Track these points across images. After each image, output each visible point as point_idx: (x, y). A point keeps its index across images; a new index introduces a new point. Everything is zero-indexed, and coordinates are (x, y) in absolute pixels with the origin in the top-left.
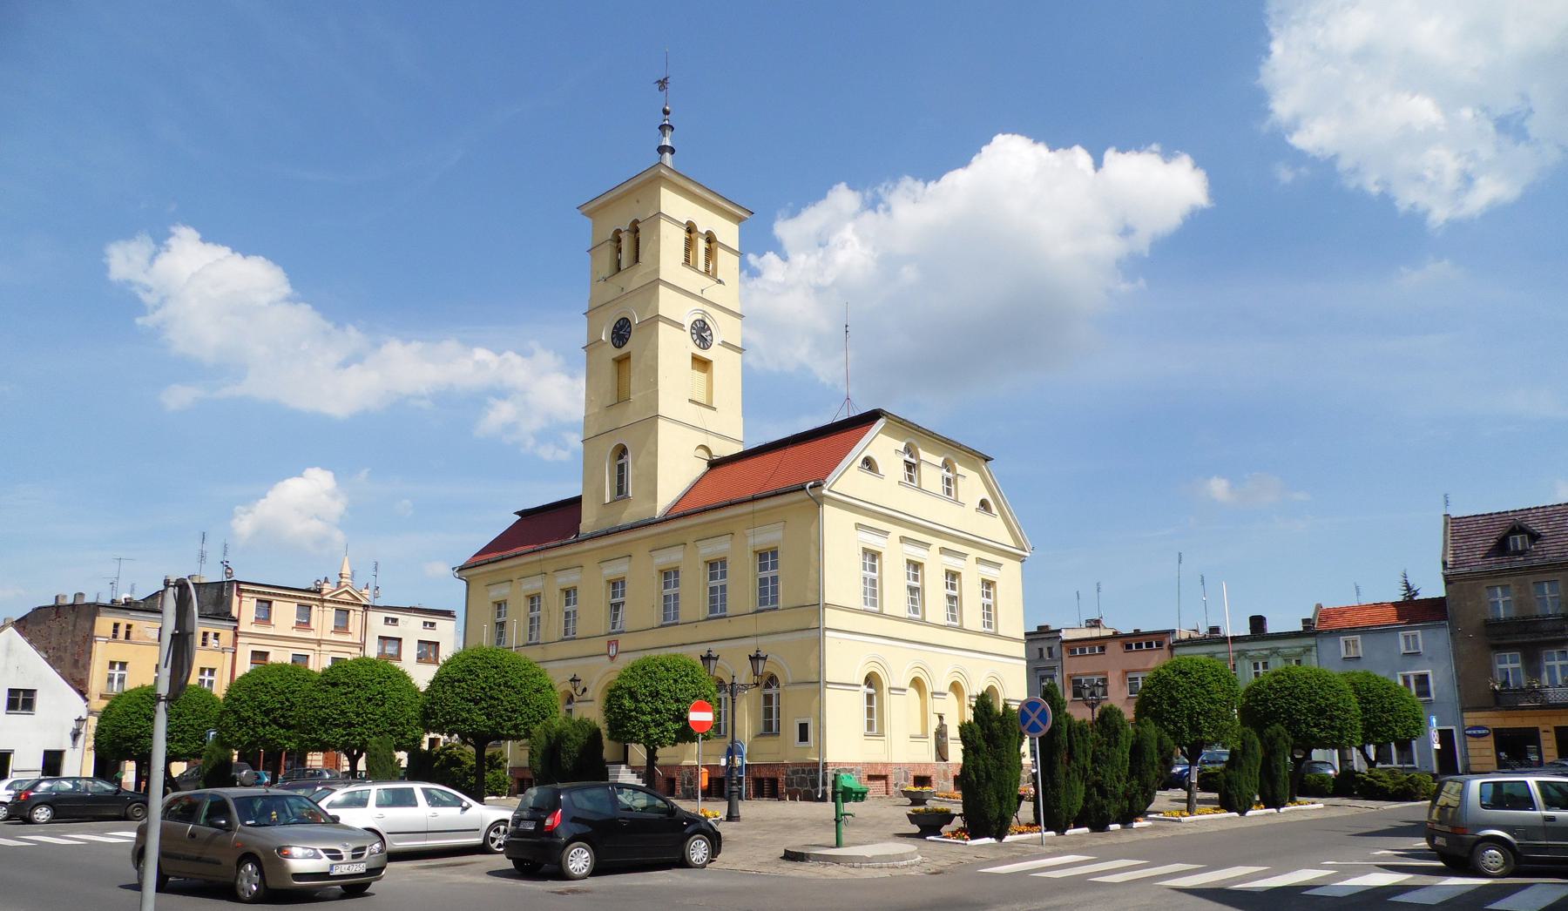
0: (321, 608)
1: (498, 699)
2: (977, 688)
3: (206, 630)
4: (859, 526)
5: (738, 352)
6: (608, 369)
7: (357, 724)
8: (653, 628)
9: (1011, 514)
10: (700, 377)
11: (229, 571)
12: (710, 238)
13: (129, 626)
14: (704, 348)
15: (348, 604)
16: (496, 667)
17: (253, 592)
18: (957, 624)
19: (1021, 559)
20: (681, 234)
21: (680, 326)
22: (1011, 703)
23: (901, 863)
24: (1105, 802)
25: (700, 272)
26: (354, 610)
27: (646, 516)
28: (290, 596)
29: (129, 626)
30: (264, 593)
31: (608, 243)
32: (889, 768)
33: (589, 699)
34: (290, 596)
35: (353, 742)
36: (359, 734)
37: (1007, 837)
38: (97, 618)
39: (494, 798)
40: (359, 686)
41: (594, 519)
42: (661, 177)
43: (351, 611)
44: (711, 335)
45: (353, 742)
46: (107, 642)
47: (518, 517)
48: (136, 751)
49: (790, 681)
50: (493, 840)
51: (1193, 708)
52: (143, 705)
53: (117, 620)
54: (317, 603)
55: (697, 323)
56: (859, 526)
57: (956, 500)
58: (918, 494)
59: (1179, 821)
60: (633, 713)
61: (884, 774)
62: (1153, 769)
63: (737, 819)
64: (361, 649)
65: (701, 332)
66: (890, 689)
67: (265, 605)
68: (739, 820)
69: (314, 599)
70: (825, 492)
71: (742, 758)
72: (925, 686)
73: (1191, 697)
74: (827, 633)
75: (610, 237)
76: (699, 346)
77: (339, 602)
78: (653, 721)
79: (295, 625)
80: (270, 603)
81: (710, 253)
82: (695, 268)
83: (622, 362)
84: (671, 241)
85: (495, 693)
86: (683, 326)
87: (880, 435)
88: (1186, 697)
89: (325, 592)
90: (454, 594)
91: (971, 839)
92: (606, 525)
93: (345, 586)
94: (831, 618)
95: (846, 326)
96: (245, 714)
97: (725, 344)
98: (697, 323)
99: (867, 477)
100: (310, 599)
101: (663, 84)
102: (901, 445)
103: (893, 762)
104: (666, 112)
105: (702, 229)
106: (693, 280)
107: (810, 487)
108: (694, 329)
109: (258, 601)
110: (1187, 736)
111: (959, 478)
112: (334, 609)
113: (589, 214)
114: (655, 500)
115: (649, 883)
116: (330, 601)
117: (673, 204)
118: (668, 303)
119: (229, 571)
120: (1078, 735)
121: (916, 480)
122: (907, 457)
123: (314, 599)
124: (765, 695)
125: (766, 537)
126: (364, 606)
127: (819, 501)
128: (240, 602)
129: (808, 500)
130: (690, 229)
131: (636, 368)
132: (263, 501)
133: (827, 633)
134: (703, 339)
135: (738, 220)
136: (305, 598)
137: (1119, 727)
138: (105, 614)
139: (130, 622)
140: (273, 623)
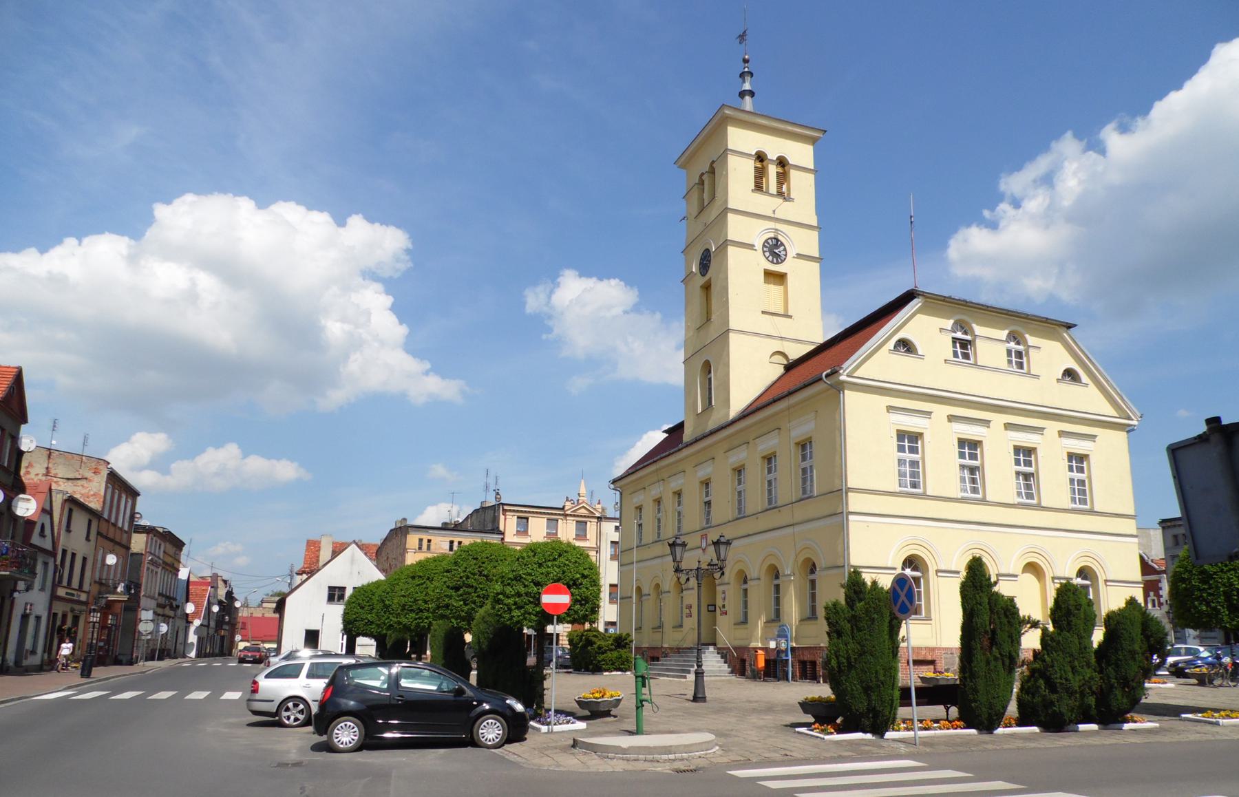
0: (565, 521)
1: (472, 586)
2: (1068, 570)
3: (452, 539)
4: (890, 409)
5: (815, 262)
6: (698, 293)
7: (425, 609)
8: (729, 522)
9: (1107, 381)
10: (775, 290)
11: (498, 496)
12: (782, 162)
13: (429, 541)
14: (778, 263)
15: (585, 516)
16: (476, 559)
17: (514, 511)
18: (1035, 502)
19: (1129, 429)
20: (750, 166)
21: (750, 247)
22: (864, 570)
23: (665, 757)
24: (1054, 697)
25: (772, 195)
26: (590, 522)
27: (722, 422)
28: (541, 513)
29: (429, 541)
30: (522, 511)
31: (696, 186)
32: (937, 653)
33: (691, 587)
34: (541, 513)
35: (422, 624)
36: (427, 618)
37: (887, 733)
38: (408, 536)
39: (619, 673)
40: (428, 579)
41: (692, 429)
42: (727, 117)
43: (588, 523)
44: (785, 250)
45: (422, 624)
46: (415, 553)
47: (666, 435)
48: (354, 631)
49: (824, 566)
50: (288, 709)
51: (1231, 585)
52: (358, 597)
53: (421, 537)
54: (562, 517)
55: (770, 241)
56: (890, 409)
57: (1029, 373)
58: (1028, 380)
59: (1217, 724)
60: (501, 596)
61: (929, 658)
62: (1135, 660)
63: (704, 699)
64: (597, 552)
65: (774, 249)
66: (937, 571)
67: (523, 520)
68: (705, 701)
69: (559, 515)
70: (843, 378)
71: (787, 641)
72: (1042, 569)
73: (1230, 570)
74: (851, 517)
75: (697, 182)
76: (772, 262)
77: (578, 516)
78: (515, 603)
79: (545, 535)
80: (527, 518)
81: (783, 177)
82: (768, 193)
83: (707, 287)
84: (739, 173)
85: (471, 581)
86: (754, 246)
87: (919, 316)
88: (1222, 571)
89: (566, 508)
90: (609, 501)
91: (838, 733)
92: (699, 433)
93: (582, 503)
94: (855, 502)
95: (911, 217)
96: (387, 603)
97: (800, 256)
98: (770, 241)
99: (904, 360)
100: (556, 514)
101: (742, 37)
102: (949, 323)
103: (943, 646)
104: (746, 61)
105: (772, 155)
106: (765, 203)
107: (827, 376)
108: (766, 247)
109: (518, 517)
110: (1225, 618)
111: (1031, 350)
112: (516, 517)
113: (683, 166)
114: (729, 407)
115: (360, 760)
116: (571, 515)
117: (742, 139)
118: (736, 228)
119: (498, 496)
120: (1002, 616)
121: (972, 357)
122: (1012, 345)
123: (559, 515)
124: (810, 580)
125: (800, 430)
126: (598, 518)
127: (840, 387)
128: (505, 519)
129: (828, 390)
130: (760, 157)
131: (715, 290)
132: (632, 449)
133: (851, 517)
134: (777, 255)
135: (813, 141)
136: (552, 514)
137: (1072, 608)
138: (413, 533)
139: (429, 538)
140: (529, 534)
